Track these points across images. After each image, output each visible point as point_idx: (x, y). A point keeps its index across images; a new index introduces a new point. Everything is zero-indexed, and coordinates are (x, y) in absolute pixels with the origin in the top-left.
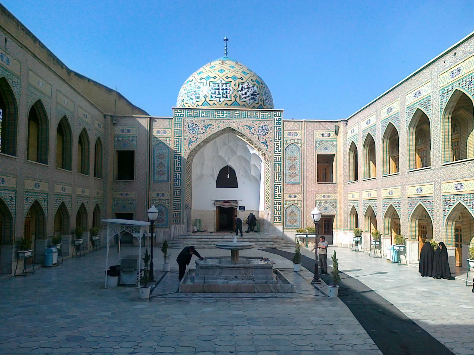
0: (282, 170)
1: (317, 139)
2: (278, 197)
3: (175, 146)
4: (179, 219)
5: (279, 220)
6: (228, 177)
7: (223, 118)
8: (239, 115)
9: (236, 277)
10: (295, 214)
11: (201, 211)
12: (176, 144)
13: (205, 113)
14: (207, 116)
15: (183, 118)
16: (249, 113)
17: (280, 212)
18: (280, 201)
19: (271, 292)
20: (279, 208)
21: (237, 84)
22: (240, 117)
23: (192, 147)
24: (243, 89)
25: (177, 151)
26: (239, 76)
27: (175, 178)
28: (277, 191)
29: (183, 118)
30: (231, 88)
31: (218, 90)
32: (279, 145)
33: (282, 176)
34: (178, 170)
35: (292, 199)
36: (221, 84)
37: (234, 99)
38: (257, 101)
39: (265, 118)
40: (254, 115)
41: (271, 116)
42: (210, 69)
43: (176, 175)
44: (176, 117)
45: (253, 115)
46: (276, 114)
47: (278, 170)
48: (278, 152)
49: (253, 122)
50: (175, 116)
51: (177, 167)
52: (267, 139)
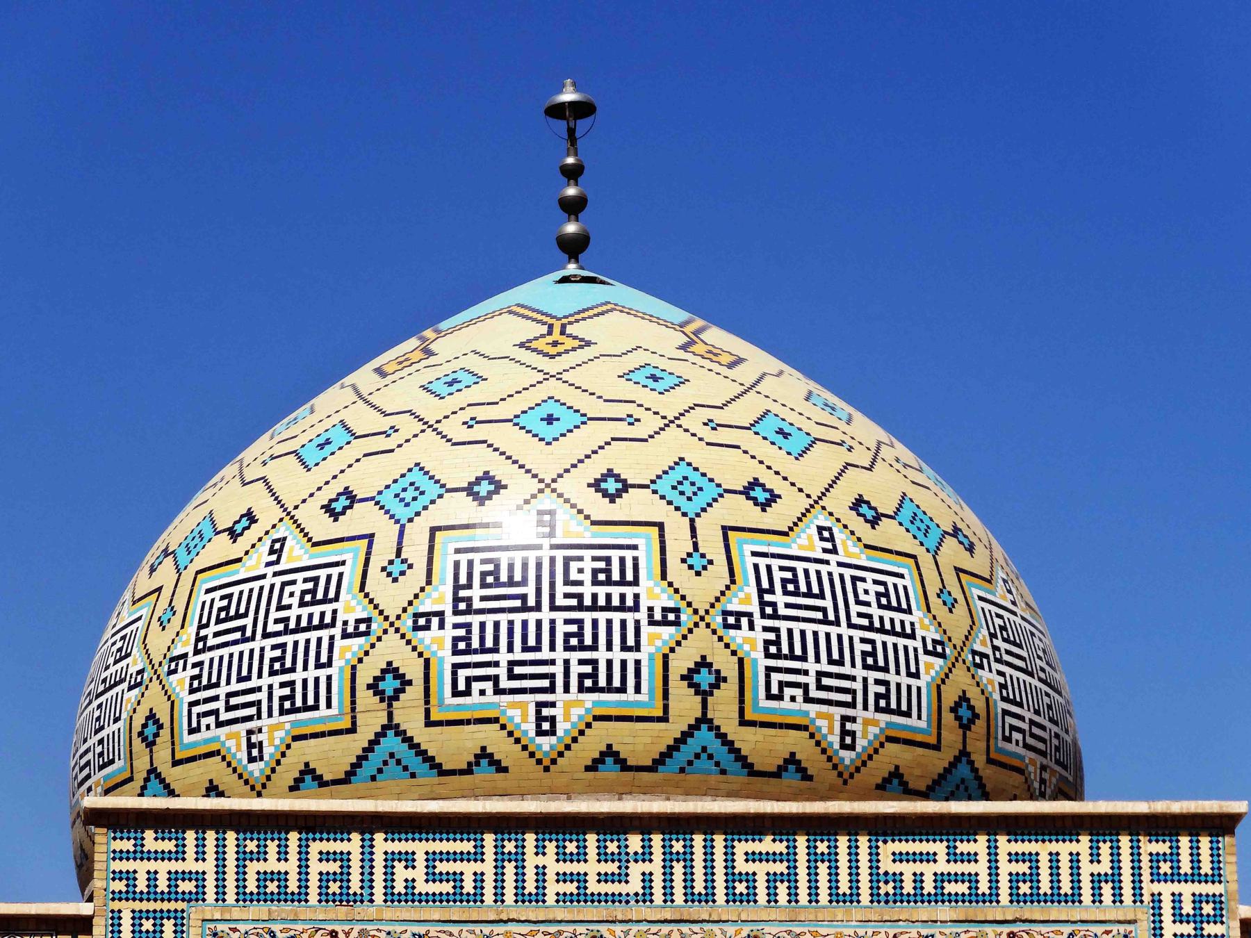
7: (619, 911)
8: (780, 868)
13: (431, 858)
14: (447, 887)
15: (195, 913)
16: (741, 848)
21: (712, 544)
22: (793, 896)
24: (779, 598)
26: (735, 471)
29: (195, 913)
30: (654, 595)
31: (518, 618)
38: (919, 723)
39: (1056, 897)
40: (942, 866)
41: (1115, 877)
42: (431, 409)
44: (127, 909)
45: (928, 870)
46: (1163, 848)
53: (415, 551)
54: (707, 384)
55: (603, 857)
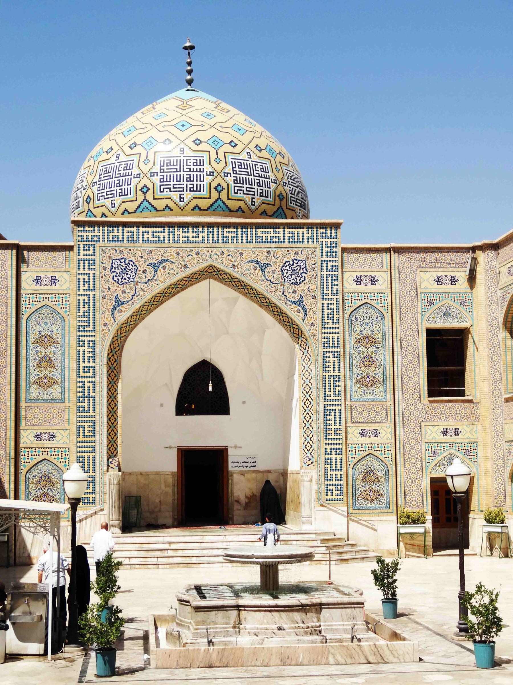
0: (342, 370)
1: (424, 291)
2: (333, 436)
3: (78, 314)
4: (91, 496)
5: (339, 492)
6: (210, 389)
7: (197, 245)
9: (280, 629)
10: (376, 477)
11: (141, 474)
12: (82, 309)
14: (157, 239)
15: (97, 245)
17: (339, 473)
18: (341, 447)
19: (365, 661)
20: (336, 463)
21: (221, 156)
22: (237, 242)
23: (122, 317)
25: (84, 327)
26: (227, 138)
27: (81, 394)
28: (332, 422)
29: (97, 245)
30: (207, 168)
31: (175, 174)
32: (335, 307)
33: (342, 384)
34: (87, 374)
35: (367, 440)
36: (182, 158)
37: (215, 195)
38: (270, 200)
41: (312, 238)
43: (83, 387)
45: (269, 235)
47: (331, 369)
48: (331, 325)
49: (268, 252)
50: (79, 241)
51: (84, 367)
52: (304, 292)
54: (221, 117)
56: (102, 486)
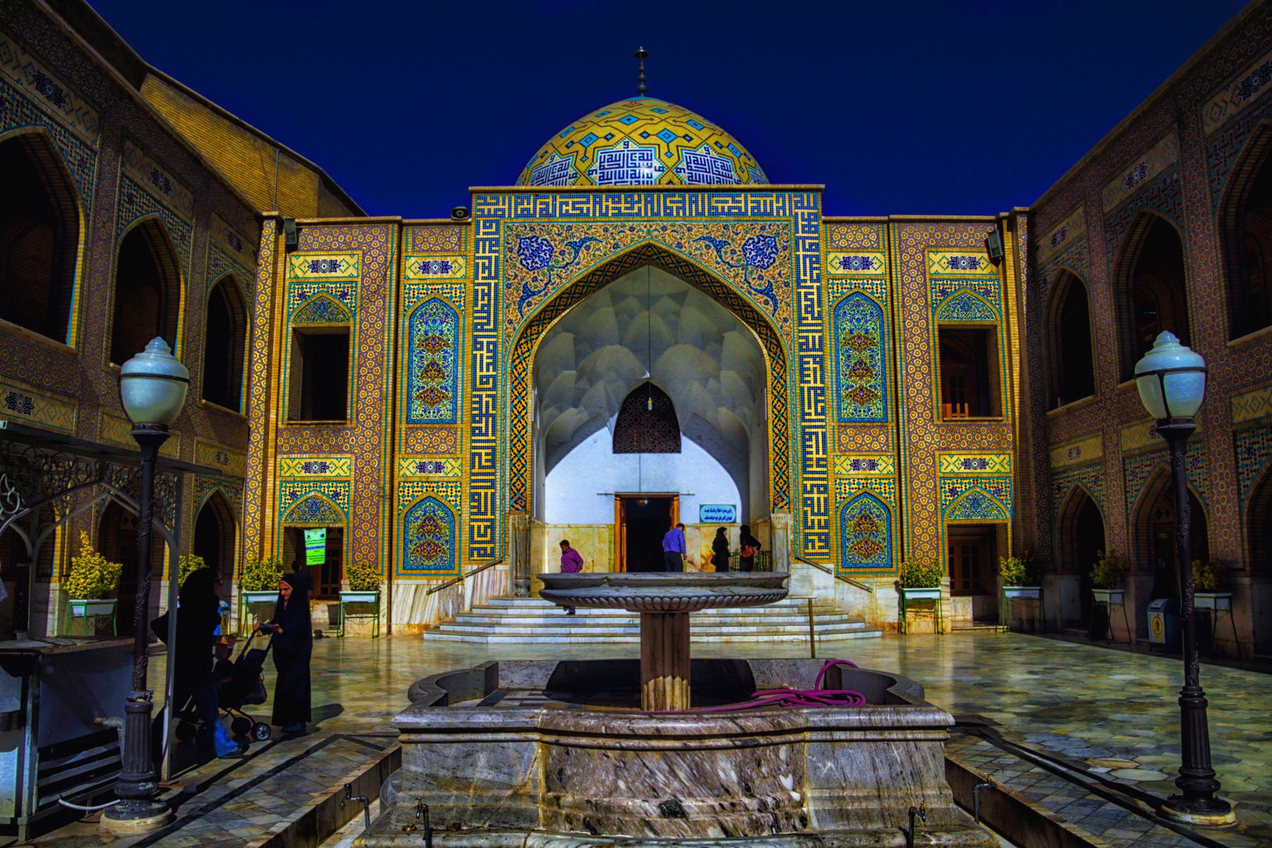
21: (673, 150)
22: (684, 213)
26: (681, 132)
35: (861, 474)
39: (765, 213)
41: (784, 208)
42: (596, 120)
45: (726, 206)
53: (589, 155)
55: (626, 202)
56: (505, 533)
